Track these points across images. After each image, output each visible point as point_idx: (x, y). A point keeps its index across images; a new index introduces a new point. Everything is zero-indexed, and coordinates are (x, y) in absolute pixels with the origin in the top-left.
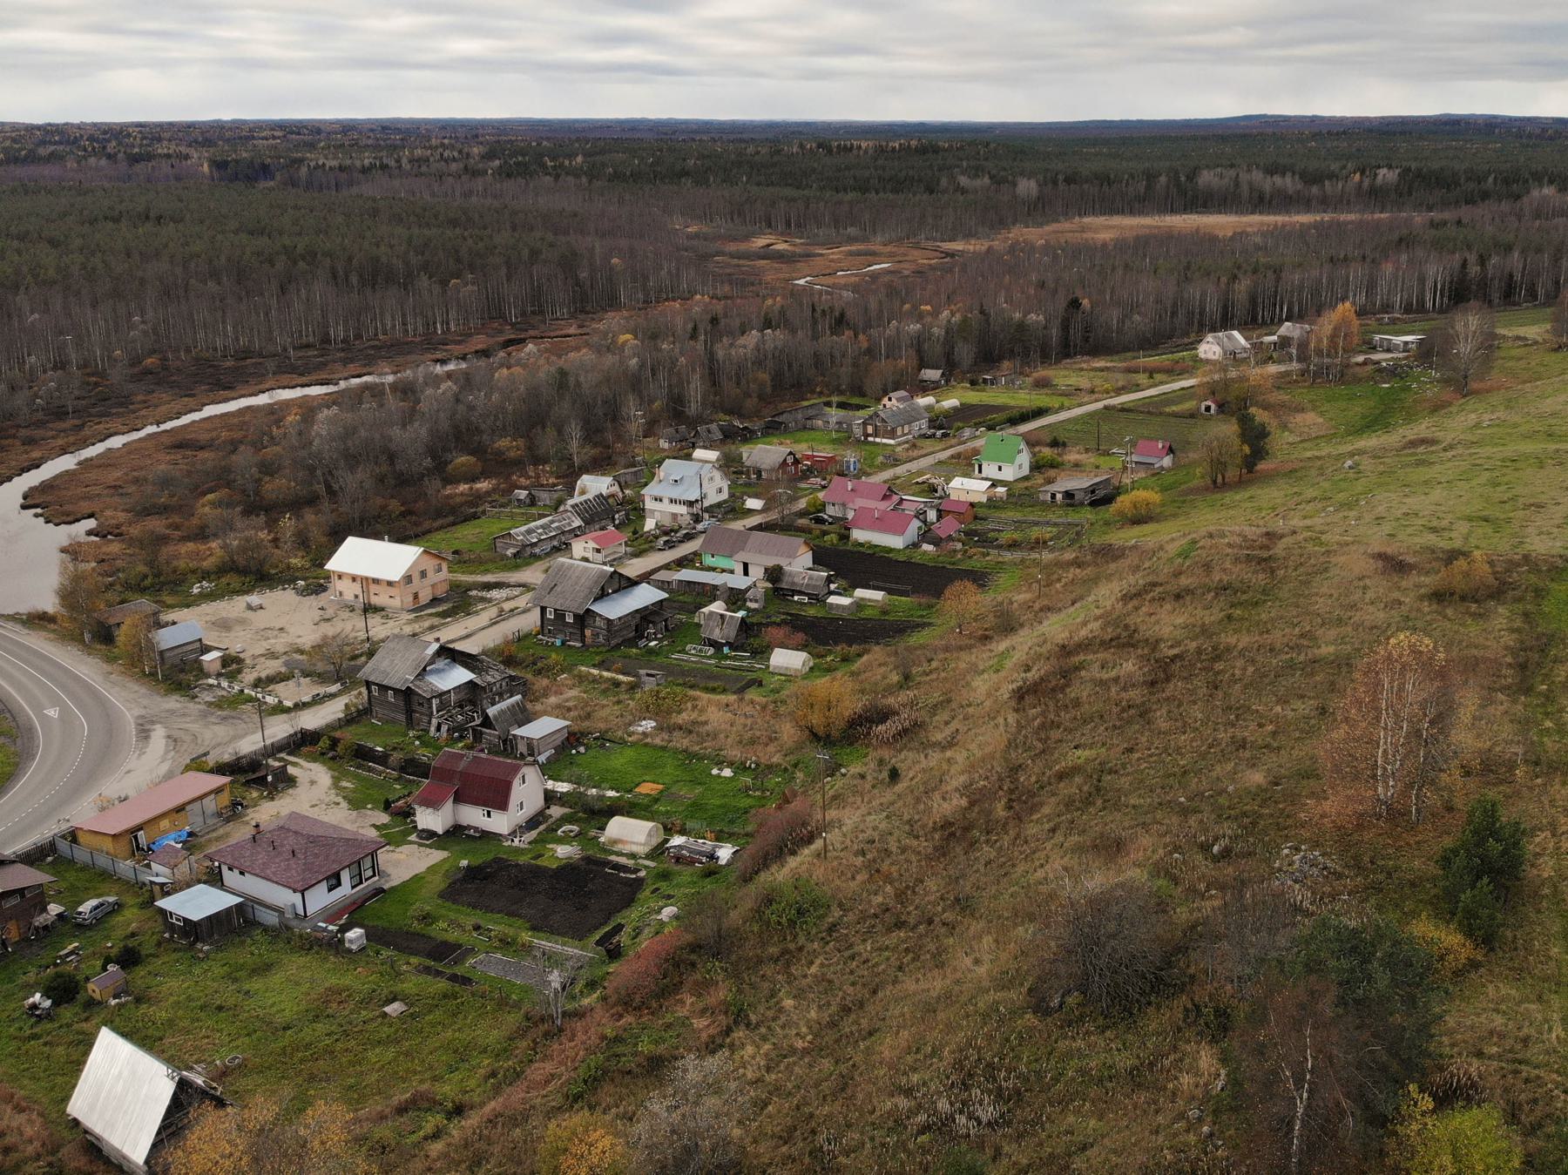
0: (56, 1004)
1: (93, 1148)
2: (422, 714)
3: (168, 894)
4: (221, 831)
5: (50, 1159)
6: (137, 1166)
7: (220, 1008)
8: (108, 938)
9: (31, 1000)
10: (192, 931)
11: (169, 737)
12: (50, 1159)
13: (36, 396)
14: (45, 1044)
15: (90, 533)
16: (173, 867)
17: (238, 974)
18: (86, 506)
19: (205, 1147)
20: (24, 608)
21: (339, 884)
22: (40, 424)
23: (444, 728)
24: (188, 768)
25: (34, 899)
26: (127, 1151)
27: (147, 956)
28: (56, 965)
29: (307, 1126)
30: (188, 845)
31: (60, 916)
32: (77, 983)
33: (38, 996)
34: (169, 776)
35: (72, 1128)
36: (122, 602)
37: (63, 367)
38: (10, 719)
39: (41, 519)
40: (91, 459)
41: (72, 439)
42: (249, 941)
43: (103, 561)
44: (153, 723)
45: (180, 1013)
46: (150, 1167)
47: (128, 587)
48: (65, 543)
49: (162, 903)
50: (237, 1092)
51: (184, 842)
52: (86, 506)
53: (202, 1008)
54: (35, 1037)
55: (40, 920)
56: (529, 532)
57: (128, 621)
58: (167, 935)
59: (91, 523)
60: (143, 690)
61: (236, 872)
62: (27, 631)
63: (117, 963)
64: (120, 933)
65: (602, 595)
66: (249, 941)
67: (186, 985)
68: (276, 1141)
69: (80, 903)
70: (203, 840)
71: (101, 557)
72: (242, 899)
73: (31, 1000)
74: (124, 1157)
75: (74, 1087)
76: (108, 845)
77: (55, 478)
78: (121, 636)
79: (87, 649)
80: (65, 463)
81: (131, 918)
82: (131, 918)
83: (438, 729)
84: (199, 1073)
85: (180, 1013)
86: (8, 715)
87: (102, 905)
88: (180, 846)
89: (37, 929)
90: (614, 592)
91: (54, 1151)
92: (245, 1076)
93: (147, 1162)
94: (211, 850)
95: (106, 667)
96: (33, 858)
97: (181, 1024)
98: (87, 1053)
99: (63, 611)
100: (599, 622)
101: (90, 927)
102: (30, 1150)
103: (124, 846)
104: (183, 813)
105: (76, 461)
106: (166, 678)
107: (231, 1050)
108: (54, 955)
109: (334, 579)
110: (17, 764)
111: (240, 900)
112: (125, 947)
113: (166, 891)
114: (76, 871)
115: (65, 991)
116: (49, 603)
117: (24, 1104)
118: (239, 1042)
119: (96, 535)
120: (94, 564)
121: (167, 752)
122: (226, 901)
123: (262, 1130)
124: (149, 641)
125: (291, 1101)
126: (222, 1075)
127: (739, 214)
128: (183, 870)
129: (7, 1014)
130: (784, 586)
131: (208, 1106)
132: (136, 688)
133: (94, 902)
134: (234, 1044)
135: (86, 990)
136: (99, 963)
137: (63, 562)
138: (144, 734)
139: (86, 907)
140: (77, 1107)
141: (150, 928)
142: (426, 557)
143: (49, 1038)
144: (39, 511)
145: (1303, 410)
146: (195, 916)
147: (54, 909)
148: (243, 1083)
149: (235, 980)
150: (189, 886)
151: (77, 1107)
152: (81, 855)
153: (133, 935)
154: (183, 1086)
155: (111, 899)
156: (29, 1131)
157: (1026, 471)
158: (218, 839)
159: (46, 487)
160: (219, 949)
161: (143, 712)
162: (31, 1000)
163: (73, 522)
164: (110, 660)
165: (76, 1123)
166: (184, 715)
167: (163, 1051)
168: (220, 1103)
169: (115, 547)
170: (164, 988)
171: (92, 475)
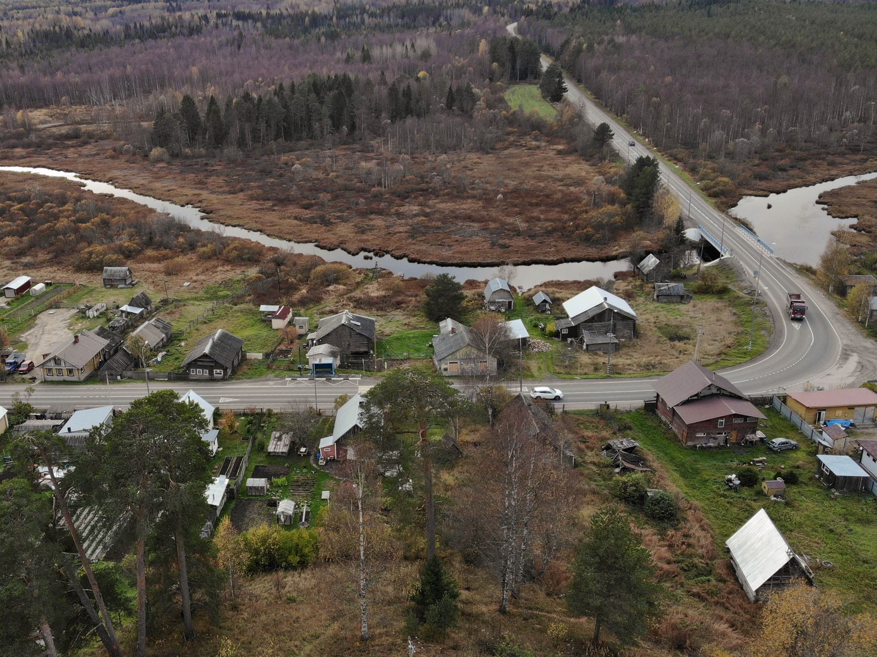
0: (742, 484)
1: (732, 568)
3: (827, 453)
4: (871, 431)
5: (708, 561)
6: (751, 590)
7: (831, 531)
8: (784, 463)
9: (730, 476)
10: (833, 481)
11: (859, 363)
12: (708, 561)
13: (844, 137)
14: (728, 502)
15: (852, 227)
16: (835, 440)
17: (849, 517)
18: (854, 210)
19: (792, 601)
20: (800, 261)
22: (843, 154)
24: (864, 385)
25: (752, 425)
26: (749, 579)
27: (802, 482)
28: (749, 464)
29: (854, 623)
30: (848, 430)
31: (761, 439)
32: (757, 479)
33: (734, 476)
34: (851, 386)
35: (725, 552)
36: (859, 273)
37: (865, 122)
38: (772, 322)
39: (826, 212)
40: (866, 182)
41: (857, 167)
42: (863, 501)
43: (855, 245)
44: (853, 351)
45: (808, 523)
46: (757, 595)
47: (865, 265)
48: (835, 229)
49: (821, 457)
50: (822, 582)
51: (847, 428)
52: (854, 210)
53: (821, 526)
54: (724, 496)
55: (749, 437)
57: (858, 286)
58: (817, 476)
59: (854, 221)
60: (853, 330)
61: (871, 458)
62: (797, 275)
63: (783, 478)
64: (790, 463)
66: (863, 501)
67: (817, 509)
68: (833, 620)
69: (775, 437)
70: (858, 431)
71: (854, 243)
72: (868, 476)
73: (730, 476)
74: (746, 582)
75: (734, 532)
76: (802, 411)
77: (841, 189)
78: (852, 293)
79: (829, 295)
80: (850, 181)
81: (800, 457)
82: (800, 457)
84: (805, 560)
85: (808, 523)
86: (771, 320)
87: (787, 443)
88: (844, 429)
89: (746, 441)
91: (712, 558)
92: (830, 576)
93: (757, 591)
94: (861, 439)
95: (837, 310)
96: (759, 402)
97: (806, 529)
98: (748, 518)
99: (822, 270)
101: (775, 452)
102: (700, 551)
103: (811, 416)
104: (853, 411)
105: (856, 181)
106: (870, 327)
107: (828, 558)
108: (751, 458)
110: (767, 348)
111: (867, 475)
112: (791, 472)
113: (826, 451)
114: (780, 419)
115: (749, 480)
116: (815, 263)
117: (706, 527)
118: (834, 555)
119: (855, 229)
120: (848, 246)
121: (855, 372)
122: (860, 473)
123: (827, 610)
124: (867, 301)
125: (850, 604)
126: (818, 568)
128: (840, 444)
129: (714, 477)
131: (802, 581)
132: (850, 328)
133: (782, 440)
134: (831, 555)
135: (761, 485)
136: (773, 474)
137: (831, 240)
138: (845, 356)
139: (778, 441)
140: (732, 543)
141: (808, 468)
143: (732, 500)
144: (826, 206)
145: (507, 264)
146: (838, 473)
147: (760, 434)
148: (826, 579)
149: (847, 520)
150: (840, 454)
151: (732, 543)
152: (785, 411)
153: (798, 467)
154: (793, 562)
155: (793, 442)
156: (703, 542)
158: (868, 434)
159: (834, 193)
160: (844, 498)
161: (849, 343)
162: (730, 476)
163: (844, 218)
164: (840, 306)
165: (728, 551)
166: (873, 353)
167: (790, 538)
168: (810, 583)
169: (864, 239)
170: (804, 505)
171: (864, 192)
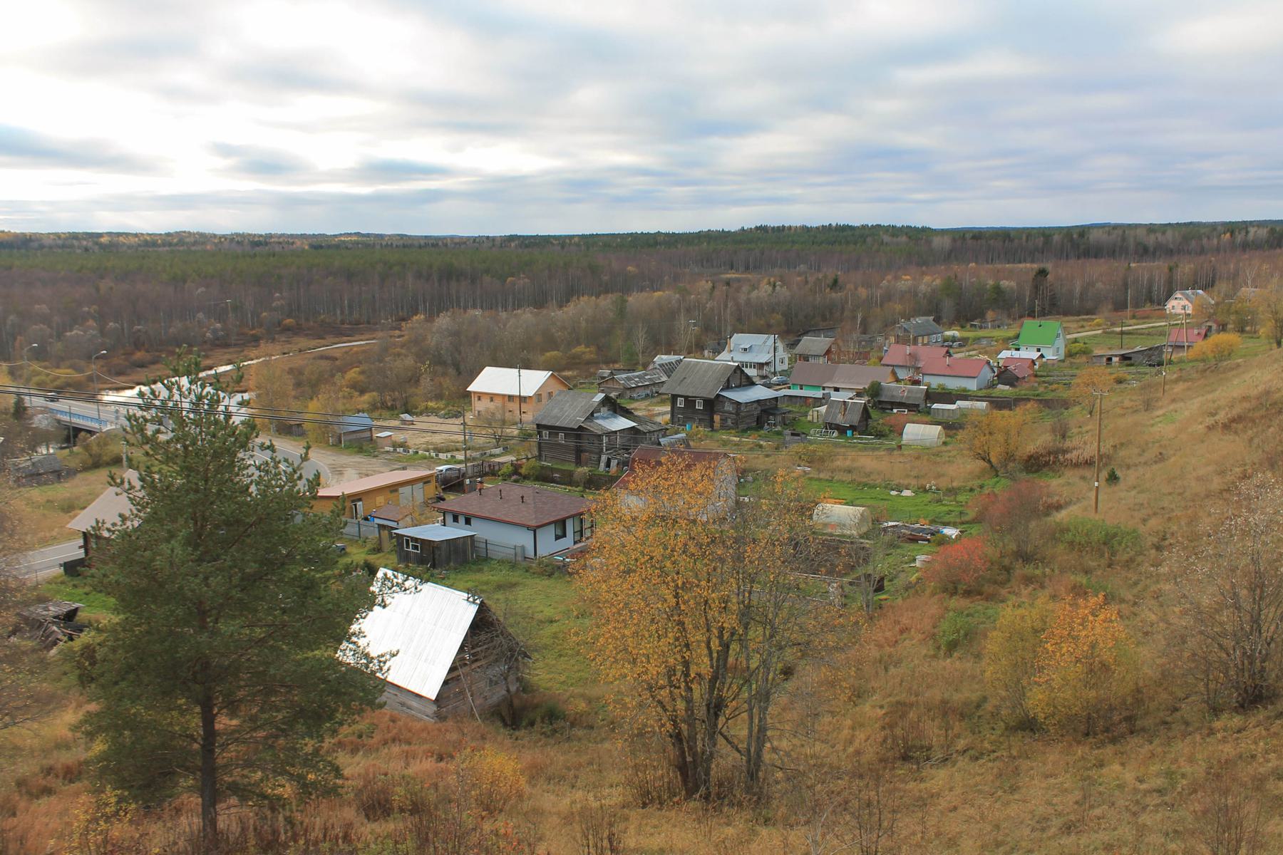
2: (591, 452)
21: (564, 535)
23: (614, 463)
56: (629, 379)
65: (728, 387)
83: (608, 465)
90: (736, 387)
100: (728, 407)
109: (474, 399)
127: (707, 261)
130: (883, 399)
142: (553, 381)
157: (1062, 355)
